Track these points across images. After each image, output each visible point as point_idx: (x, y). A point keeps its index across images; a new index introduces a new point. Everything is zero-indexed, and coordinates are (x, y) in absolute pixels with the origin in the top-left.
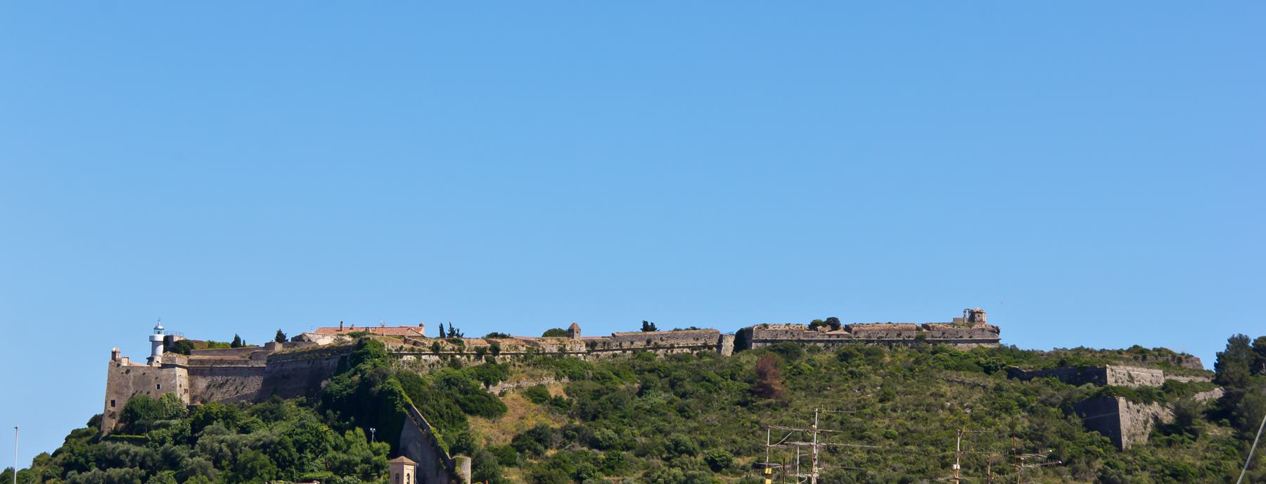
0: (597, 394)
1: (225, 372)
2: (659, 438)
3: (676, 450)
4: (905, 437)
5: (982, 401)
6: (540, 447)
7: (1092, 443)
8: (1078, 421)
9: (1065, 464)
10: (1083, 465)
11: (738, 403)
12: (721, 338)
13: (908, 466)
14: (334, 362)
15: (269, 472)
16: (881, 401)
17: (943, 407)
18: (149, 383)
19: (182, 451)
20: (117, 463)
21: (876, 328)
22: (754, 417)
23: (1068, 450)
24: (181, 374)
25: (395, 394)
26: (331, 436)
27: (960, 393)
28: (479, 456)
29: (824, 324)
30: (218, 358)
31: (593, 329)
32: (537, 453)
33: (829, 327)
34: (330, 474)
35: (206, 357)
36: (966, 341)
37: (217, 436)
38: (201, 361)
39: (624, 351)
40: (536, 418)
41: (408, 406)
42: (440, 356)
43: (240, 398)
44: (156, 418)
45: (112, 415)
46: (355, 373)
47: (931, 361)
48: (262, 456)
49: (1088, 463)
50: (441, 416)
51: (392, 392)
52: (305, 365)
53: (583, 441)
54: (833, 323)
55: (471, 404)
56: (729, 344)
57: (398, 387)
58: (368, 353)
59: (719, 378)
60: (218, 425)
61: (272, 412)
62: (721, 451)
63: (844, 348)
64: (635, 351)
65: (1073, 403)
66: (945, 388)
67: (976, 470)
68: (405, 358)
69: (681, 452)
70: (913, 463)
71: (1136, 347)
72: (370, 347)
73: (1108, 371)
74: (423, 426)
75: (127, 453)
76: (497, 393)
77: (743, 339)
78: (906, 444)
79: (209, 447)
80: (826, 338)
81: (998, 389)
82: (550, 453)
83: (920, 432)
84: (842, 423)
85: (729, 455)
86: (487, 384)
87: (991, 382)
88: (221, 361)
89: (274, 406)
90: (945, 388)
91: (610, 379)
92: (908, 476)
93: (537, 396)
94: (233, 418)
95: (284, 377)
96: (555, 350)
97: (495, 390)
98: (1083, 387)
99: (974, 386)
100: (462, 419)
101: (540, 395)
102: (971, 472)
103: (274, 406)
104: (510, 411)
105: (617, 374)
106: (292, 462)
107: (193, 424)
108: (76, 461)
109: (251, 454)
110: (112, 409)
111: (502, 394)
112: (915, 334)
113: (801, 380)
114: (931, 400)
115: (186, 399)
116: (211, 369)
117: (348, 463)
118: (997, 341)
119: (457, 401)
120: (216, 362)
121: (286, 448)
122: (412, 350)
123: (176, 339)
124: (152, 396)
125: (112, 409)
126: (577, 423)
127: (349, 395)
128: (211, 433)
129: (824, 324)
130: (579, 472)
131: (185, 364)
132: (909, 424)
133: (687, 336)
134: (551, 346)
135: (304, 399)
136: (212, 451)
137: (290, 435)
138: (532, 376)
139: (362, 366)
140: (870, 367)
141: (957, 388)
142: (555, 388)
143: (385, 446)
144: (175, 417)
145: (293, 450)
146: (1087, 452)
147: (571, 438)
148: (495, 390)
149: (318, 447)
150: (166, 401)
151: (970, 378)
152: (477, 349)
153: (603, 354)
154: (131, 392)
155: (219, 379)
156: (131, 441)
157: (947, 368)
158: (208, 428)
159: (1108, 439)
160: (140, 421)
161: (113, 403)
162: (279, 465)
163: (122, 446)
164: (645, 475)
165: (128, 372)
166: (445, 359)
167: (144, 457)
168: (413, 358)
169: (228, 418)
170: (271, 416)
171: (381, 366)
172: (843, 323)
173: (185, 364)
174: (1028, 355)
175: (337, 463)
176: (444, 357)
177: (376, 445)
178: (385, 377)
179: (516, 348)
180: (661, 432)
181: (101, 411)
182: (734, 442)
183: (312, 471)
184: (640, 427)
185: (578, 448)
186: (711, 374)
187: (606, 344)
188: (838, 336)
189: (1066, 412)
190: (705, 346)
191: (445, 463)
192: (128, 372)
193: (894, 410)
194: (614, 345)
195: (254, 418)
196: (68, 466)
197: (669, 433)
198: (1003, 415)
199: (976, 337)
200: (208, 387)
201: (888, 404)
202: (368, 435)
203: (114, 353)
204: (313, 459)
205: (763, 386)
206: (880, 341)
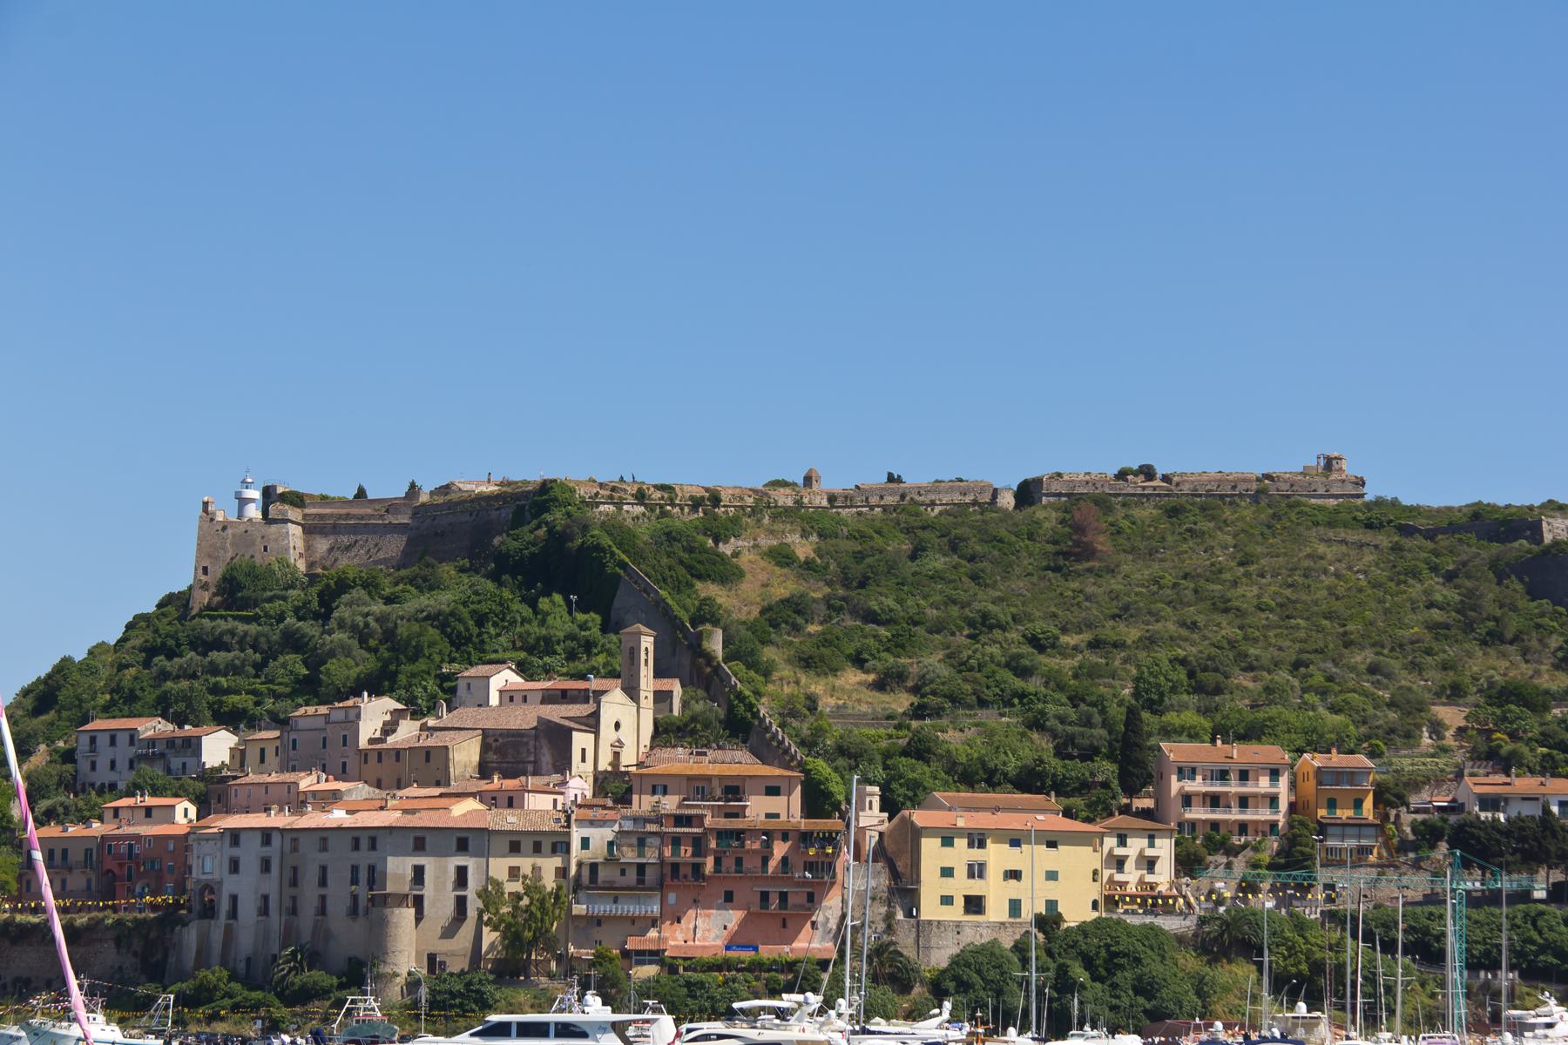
0: (859, 557)
1: (354, 529)
2: (955, 611)
3: (983, 624)
4: (1286, 609)
5: (1377, 565)
6: (800, 620)
7: (1542, 615)
8: (1519, 587)
9: (1511, 643)
10: (1534, 643)
11: (1047, 568)
12: (995, 493)
13: (1297, 646)
14: (508, 513)
15: (440, 652)
16: (1241, 564)
17: (1325, 572)
18: (253, 543)
19: (309, 628)
20: (219, 644)
21: (1205, 478)
22: (1075, 585)
23: (1513, 624)
24: (295, 531)
25: (603, 550)
26: (521, 609)
27: (1345, 555)
28: (70, 869)
29: (1136, 473)
30: (343, 511)
31: (835, 480)
32: (796, 628)
33: (1142, 477)
34: (523, 655)
35: (328, 511)
36: (1321, 496)
37: (357, 608)
38: (322, 517)
39: (872, 508)
40: (784, 586)
41: (623, 565)
42: (646, 506)
43: (375, 563)
44: (264, 589)
45: (205, 587)
46: (539, 527)
47: (1293, 516)
48: (431, 631)
49: (1540, 641)
50: (664, 580)
51: (598, 548)
52: (466, 518)
53: (854, 613)
54: (1147, 472)
55: (699, 566)
56: (1007, 501)
57: (606, 541)
58: (556, 499)
59: (1013, 538)
60: (358, 593)
61: (425, 580)
62: (1039, 626)
63: (1173, 501)
64: (885, 508)
65: (1508, 564)
66: (1322, 549)
67: (1392, 650)
68: (602, 508)
69: (991, 628)
70: (1305, 641)
71: (1550, 501)
72: (557, 492)
73: (1544, 525)
74: (647, 589)
75: (232, 633)
76: (729, 553)
77: (1027, 493)
78: (1288, 617)
79: (349, 621)
80: (1139, 491)
81: (1396, 548)
82: (812, 628)
83: (1305, 603)
84: (1196, 592)
85: (1056, 631)
86: (716, 541)
87: (1383, 540)
88: (348, 516)
89: (426, 571)
90: (1322, 549)
91: (871, 538)
92: (1305, 656)
93: (782, 557)
94: (377, 586)
95: (436, 534)
96: (790, 503)
97: (726, 549)
98: (1516, 544)
99: (1361, 546)
100: (692, 586)
101: (787, 557)
102: (1386, 651)
103: (426, 571)
104: (748, 577)
105: (879, 532)
106: (469, 639)
107: (320, 595)
108: (164, 644)
109: (416, 627)
110: (204, 578)
111: (736, 554)
112: (1254, 486)
113: (1121, 540)
114: (1307, 563)
115: (302, 566)
116: (335, 526)
117: (547, 640)
118: (1362, 496)
119: (681, 562)
120: (340, 517)
121: (460, 620)
122: (611, 497)
123: (280, 490)
124: (258, 560)
125: (204, 578)
126: (841, 592)
127: (533, 555)
128: (350, 604)
129: (1136, 473)
130: (859, 653)
131: (299, 519)
132: (1288, 592)
133: (951, 490)
134: (784, 498)
135: (466, 563)
136: (354, 628)
137: (465, 604)
138: (772, 532)
139: (548, 517)
140: (1212, 525)
141: (1337, 549)
142: (804, 549)
143: (594, 618)
144: (292, 587)
145: (471, 623)
146: (1538, 626)
147: (839, 610)
148: (726, 549)
149: (503, 618)
150: (276, 567)
151: (1353, 536)
152: (692, 498)
153: (844, 512)
154: (230, 555)
155: (345, 540)
156: (235, 618)
157: (1316, 524)
158: (345, 597)
159: (1563, 610)
160: (245, 593)
161: (205, 570)
162: (452, 643)
163: (223, 625)
164: (949, 656)
165: (224, 528)
166: (652, 511)
167: (256, 639)
168: (612, 508)
169: (370, 585)
170: (429, 585)
171: (577, 514)
172: (1160, 472)
173: (299, 519)
174: (1415, 511)
175: (531, 641)
176: (651, 508)
177: (580, 617)
178: (585, 528)
179: (742, 499)
180: (954, 602)
181: (180, 585)
182: (1055, 615)
183: (496, 651)
184: (925, 597)
185: (850, 622)
186: (1003, 533)
187: (848, 500)
188: (1155, 488)
189: (1500, 578)
190: (975, 503)
191: (685, 637)
192: (224, 528)
193: (1262, 576)
194: (858, 500)
195: (401, 586)
196: (151, 651)
197: (969, 604)
198: (1411, 581)
199: (1334, 491)
200: (331, 550)
201: (1252, 568)
202: (569, 603)
203: (206, 504)
204: (499, 635)
205: (1077, 544)
206: (1209, 494)
